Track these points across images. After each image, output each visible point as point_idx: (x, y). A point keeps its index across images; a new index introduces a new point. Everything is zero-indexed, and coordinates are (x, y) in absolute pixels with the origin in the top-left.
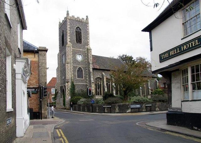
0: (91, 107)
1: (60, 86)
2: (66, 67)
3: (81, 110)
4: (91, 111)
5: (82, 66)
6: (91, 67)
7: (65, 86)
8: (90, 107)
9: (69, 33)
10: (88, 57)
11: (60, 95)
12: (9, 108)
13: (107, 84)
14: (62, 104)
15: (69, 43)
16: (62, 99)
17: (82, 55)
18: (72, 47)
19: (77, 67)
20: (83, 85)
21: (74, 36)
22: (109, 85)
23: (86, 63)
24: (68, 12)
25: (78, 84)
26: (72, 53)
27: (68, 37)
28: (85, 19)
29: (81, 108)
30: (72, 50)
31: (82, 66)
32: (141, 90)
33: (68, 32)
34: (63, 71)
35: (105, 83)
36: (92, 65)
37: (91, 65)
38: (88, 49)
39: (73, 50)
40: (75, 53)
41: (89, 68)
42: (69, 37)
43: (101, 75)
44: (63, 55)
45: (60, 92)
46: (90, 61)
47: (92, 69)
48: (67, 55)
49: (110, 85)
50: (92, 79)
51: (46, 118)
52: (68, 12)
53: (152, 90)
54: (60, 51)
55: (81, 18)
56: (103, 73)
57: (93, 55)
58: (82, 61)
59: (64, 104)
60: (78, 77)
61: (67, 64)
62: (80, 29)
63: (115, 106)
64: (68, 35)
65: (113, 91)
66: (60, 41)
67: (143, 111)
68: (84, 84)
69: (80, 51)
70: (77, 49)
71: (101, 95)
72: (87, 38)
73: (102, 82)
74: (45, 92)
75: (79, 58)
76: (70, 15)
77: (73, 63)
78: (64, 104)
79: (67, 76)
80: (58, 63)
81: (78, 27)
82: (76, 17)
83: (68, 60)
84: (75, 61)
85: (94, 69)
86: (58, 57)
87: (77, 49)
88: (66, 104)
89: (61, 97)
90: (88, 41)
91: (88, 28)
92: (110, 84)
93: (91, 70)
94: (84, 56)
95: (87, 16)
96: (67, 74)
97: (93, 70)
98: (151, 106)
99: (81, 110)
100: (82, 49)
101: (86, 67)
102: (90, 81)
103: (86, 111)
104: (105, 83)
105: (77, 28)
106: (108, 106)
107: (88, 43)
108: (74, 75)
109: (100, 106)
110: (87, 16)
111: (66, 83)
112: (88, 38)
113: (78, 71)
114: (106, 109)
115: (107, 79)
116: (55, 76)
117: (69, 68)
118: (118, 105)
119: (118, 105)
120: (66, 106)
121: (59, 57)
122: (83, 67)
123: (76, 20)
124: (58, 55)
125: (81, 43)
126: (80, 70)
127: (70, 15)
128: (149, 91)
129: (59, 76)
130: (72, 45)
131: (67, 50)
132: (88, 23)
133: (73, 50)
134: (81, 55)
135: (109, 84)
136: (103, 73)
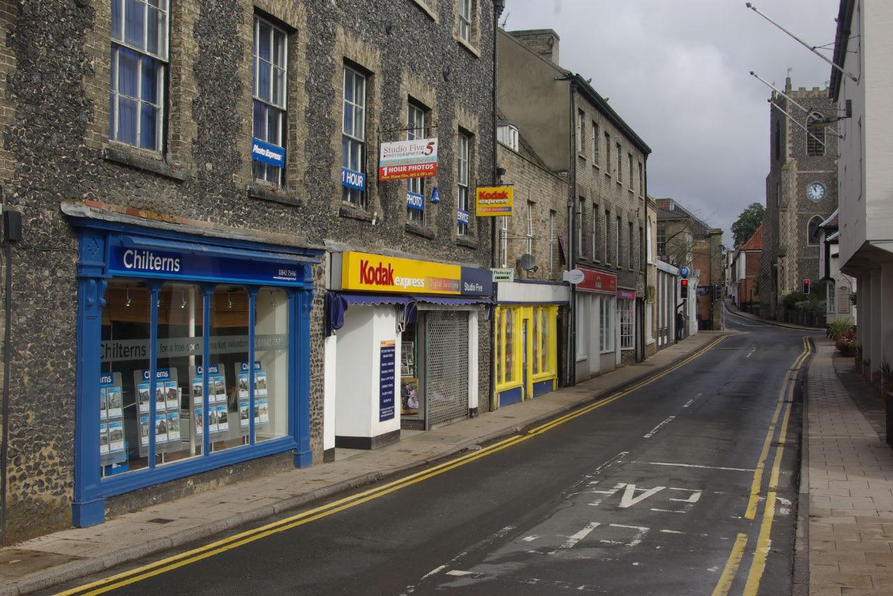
3: (385, 364)
9: (790, 135)
12: (750, 514)
15: (789, 159)
17: (824, 185)
24: (788, 80)
26: (796, 183)
27: (788, 145)
32: (111, 430)
40: (803, 184)
42: (791, 145)
51: (719, 329)
52: (788, 80)
64: (788, 138)
70: (810, 172)
74: (718, 293)
75: (816, 193)
82: (809, 89)
84: (804, 201)
87: (810, 172)
99: (385, 364)
100: (825, 169)
103: (805, 323)
111: (779, 259)
124: (768, 179)
134: (820, 184)
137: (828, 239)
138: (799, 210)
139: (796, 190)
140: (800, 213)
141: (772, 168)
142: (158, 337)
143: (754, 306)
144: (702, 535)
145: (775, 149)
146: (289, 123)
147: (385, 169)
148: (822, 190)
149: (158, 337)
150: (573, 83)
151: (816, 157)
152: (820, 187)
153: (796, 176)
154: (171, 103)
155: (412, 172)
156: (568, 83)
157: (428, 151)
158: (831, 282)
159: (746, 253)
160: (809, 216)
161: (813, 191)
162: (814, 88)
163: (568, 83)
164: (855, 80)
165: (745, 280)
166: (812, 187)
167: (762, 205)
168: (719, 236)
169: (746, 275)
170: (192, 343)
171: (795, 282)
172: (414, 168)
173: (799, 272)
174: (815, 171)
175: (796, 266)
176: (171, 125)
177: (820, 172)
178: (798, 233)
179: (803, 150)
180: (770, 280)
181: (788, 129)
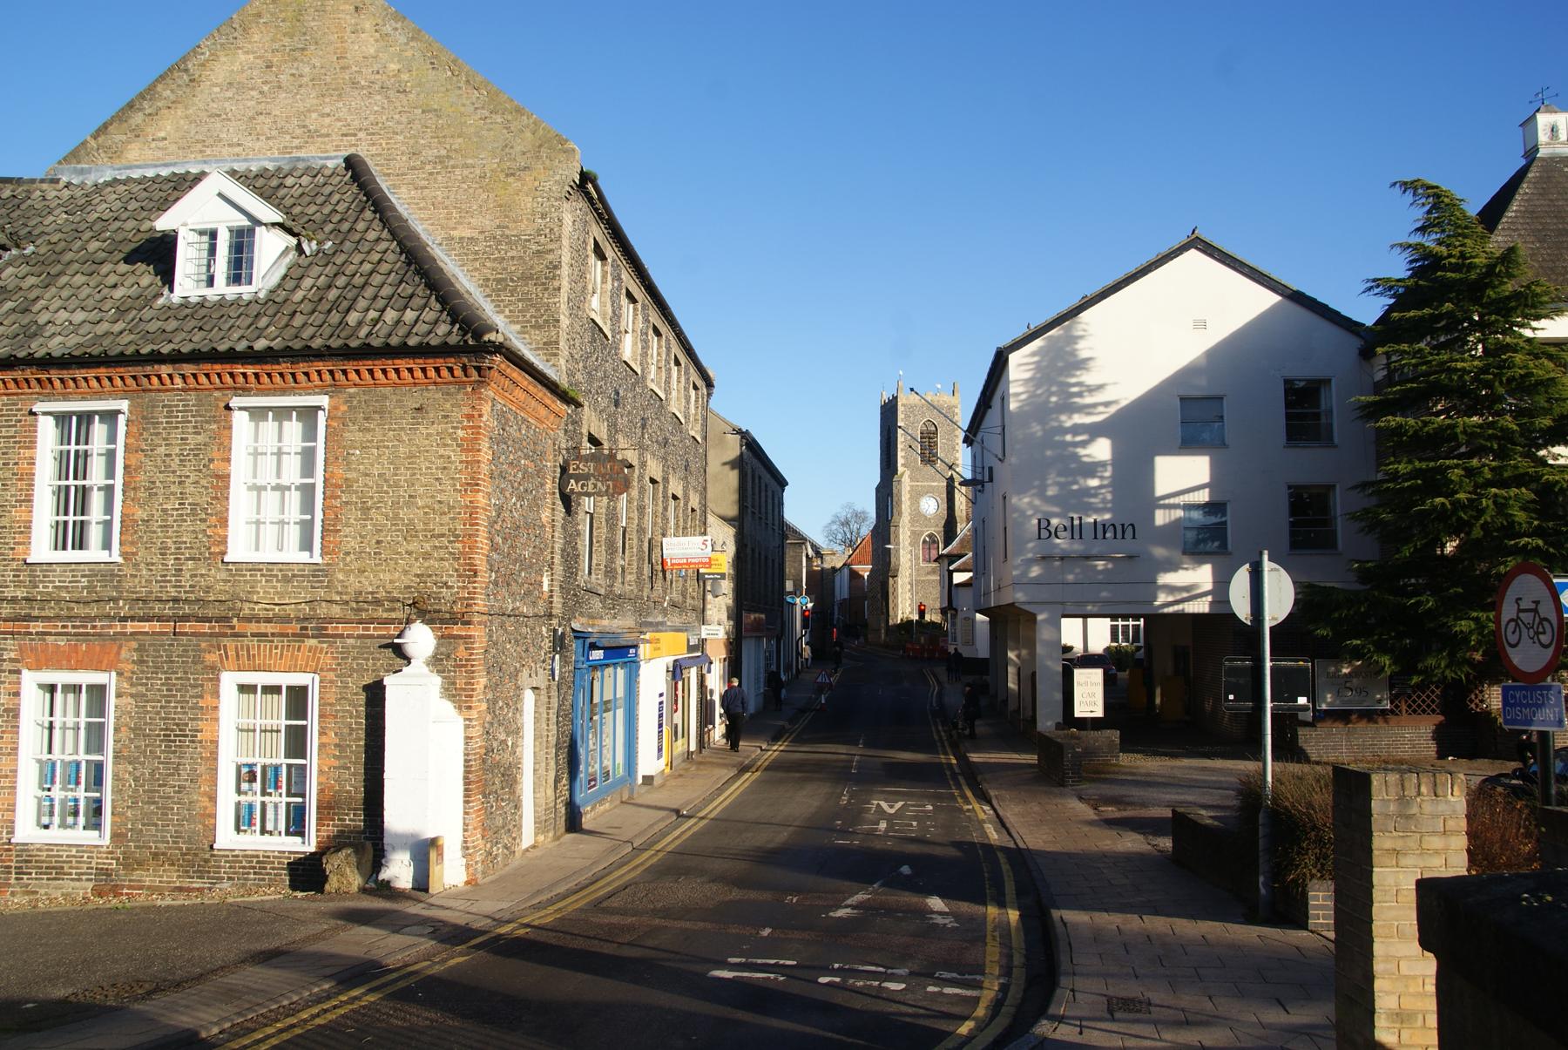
15: (900, 469)
42: (903, 454)
64: (900, 446)
84: (917, 516)
124: (878, 489)
137: (951, 568)
138: (912, 526)
139: (908, 503)
141: (881, 477)
142: (105, 686)
144: (831, 914)
145: (884, 457)
146: (627, 536)
147: (669, 561)
149: (105, 686)
150: (742, 438)
153: (908, 488)
154: (594, 541)
155: (691, 563)
156: (738, 437)
157: (704, 547)
158: (953, 612)
160: (921, 533)
163: (738, 437)
164: (1000, 460)
167: (868, 511)
172: (693, 561)
176: (594, 556)
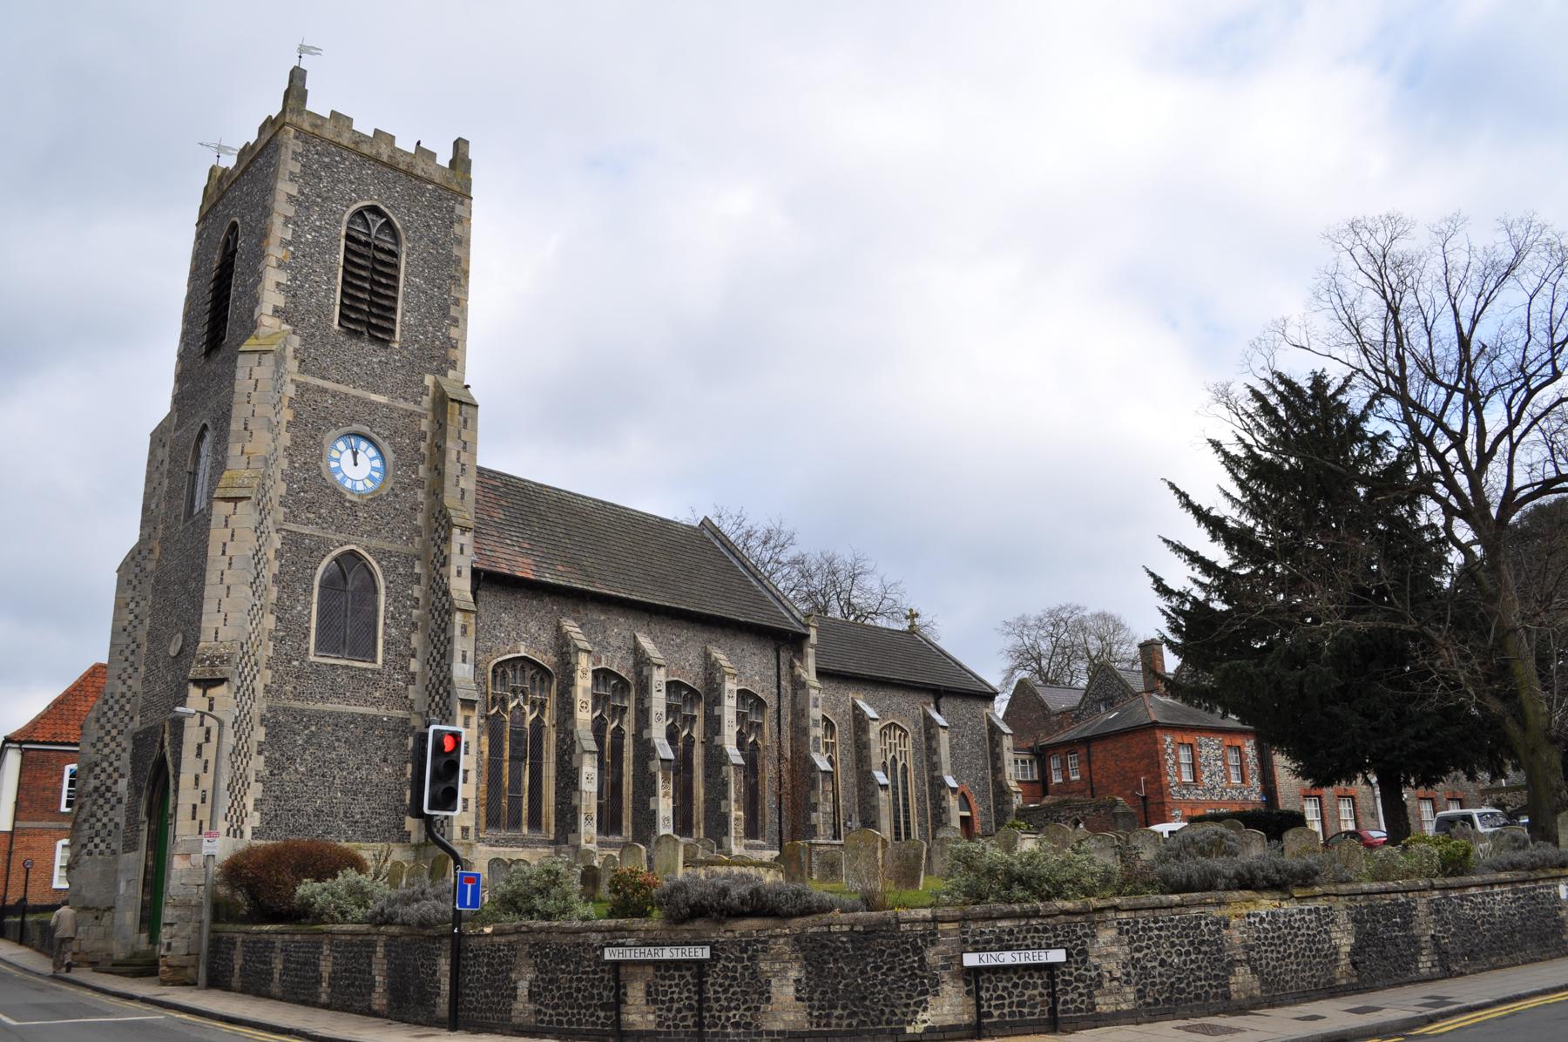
0: (444, 965)
1: (136, 724)
2: (217, 535)
4: (443, 1006)
5: (375, 543)
6: (462, 556)
7: (178, 724)
8: (432, 957)
9: (285, 244)
10: (438, 471)
11: (120, 817)
13: (598, 727)
14: (128, 917)
15: (269, 323)
16: (135, 862)
18: (292, 365)
19: (322, 546)
20: (375, 719)
21: (331, 270)
22: (618, 734)
23: (420, 520)
24: (297, 78)
25: (318, 717)
26: (287, 415)
27: (273, 276)
28: (444, 158)
29: (326, 968)
30: (290, 390)
31: (375, 543)
33: (279, 231)
34: (184, 583)
35: (584, 717)
36: (467, 539)
37: (458, 538)
38: (442, 401)
39: (302, 388)
41: (445, 563)
42: (283, 277)
43: (546, 637)
44: (201, 437)
45: (122, 785)
46: (450, 499)
47: (467, 573)
48: (236, 426)
49: (628, 743)
50: (462, 672)
52: (297, 78)
53: (965, 802)
54: (178, 400)
55: (405, 144)
56: (571, 627)
57: (481, 471)
58: (376, 498)
59: (150, 919)
60: (320, 646)
61: (221, 509)
62: (389, 224)
63: (751, 948)
65: (654, 793)
66: (188, 318)
67: (1104, 1004)
68: (381, 711)
69: (367, 403)
70: (342, 388)
71: (535, 821)
72: (444, 310)
73: (551, 703)
76: (318, 104)
77: (295, 503)
78: (150, 919)
79: (210, 621)
80: (146, 509)
81: (374, 210)
82: (364, 126)
83: (238, 471)
85: (484, 579)
86: (152, 452)
87: (342, 388)
88: (168, 914)
89: (130, 846)
90: (454, 332)
91: (457, 229)
92: (629, 728)
93: (461, 587)
94: (398, 451)
95: (460, 146)
96: (209, 607)
97: (474, 593)
98: (699, 963)
101: (409, 560)
102: (441, 685)
104: (584, 717)
105: (359, 213)
106: (667, 954)
107: (453, 354)
108: (290, 627)
109: (561, 955)
110: (460, 146)
111: (194, 693)
112: (453, 311)
113: (327, 584)
114: (636, 993)
115: (601, 675)
116: (105, 661)
117: (244, 546)
118: (798, 940)
119: (798, 940)
120: (165, 934)
121: (164, 454)
122: (382, 555)
123: (365, 149)
124: (158, 438)
125: (385, 343)
126: (353, 583)
127: (318, 104)
128: (945, 810)
129: (141, 635)
130: (296, 341)
131: (242, 383)
132: (464, 195)
133: (302, 388)
135: (618, 729)
136: (571, 627)
140: (293, 527)
143: (30, 918)
148: (377, 463)
151: (367, 347)
152: (372, 452)
159: (24, 753)
160: (322, 546)
161: (348, 456)
162: (377, 132)
165: (12, 833)
166: (341, 445)
168: (18, 938)
169: (16, 818)
170: (1264, 988)
171: (250, 803)
173: (268, 762)
174: (359, 392)
175: (260, 734)
177: (374, 397)
178: (279, 606)
179: (323, 311)
180: (122, 808)
181: (277, 221)
